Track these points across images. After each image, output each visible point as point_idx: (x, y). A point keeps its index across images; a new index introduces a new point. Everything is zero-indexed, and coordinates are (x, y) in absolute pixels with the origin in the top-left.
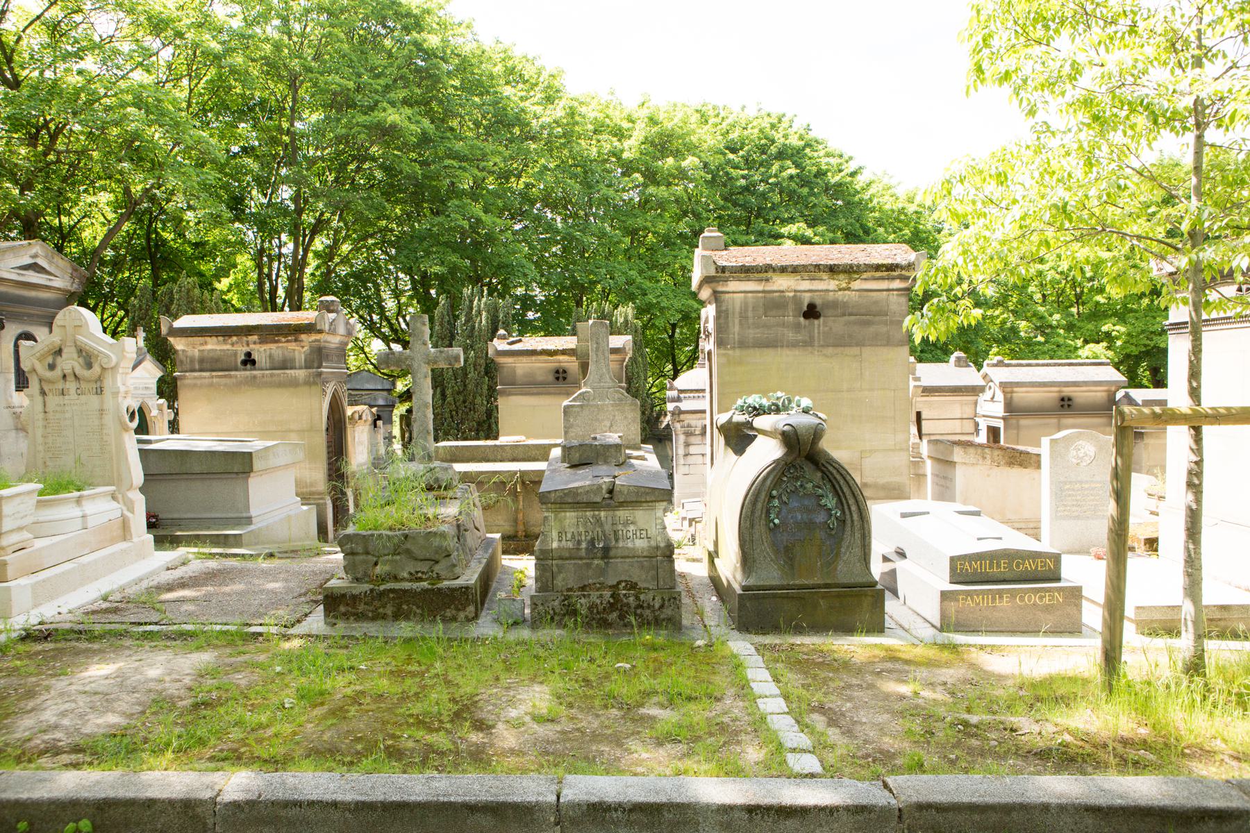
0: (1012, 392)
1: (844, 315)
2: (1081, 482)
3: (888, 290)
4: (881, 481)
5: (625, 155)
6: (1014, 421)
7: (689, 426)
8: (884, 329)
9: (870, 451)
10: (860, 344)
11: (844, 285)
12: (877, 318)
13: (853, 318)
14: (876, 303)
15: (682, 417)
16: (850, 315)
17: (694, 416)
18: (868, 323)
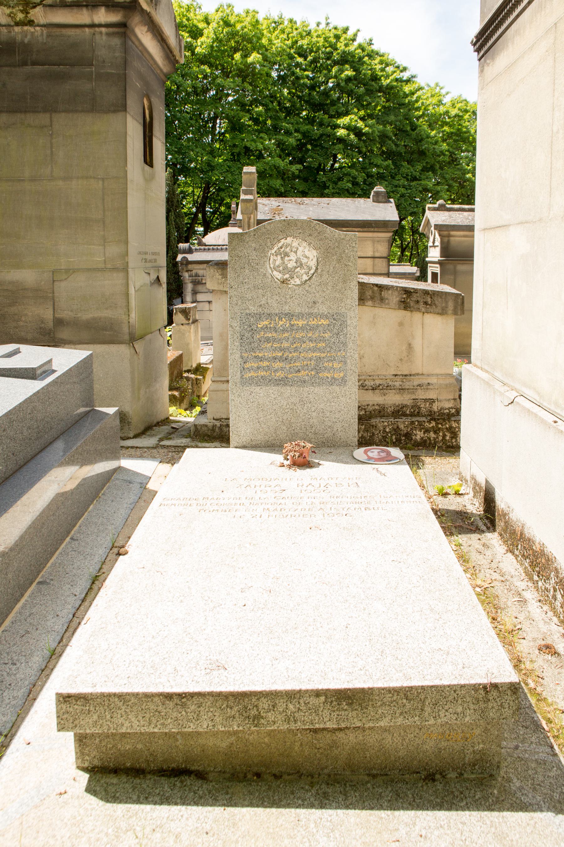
0: (449, 236)
1: (24, 63)
2: (290, 316)
3: (93, 26)
4: (86, 316)
5: (198, 50)
6: (450, 267)
7: (197, 275)
8: (87, 86)
9: (67, 271)
10: (51, 108)
11: (20, 16)
12: (76, 70)
13: (38, 68)
14: (75, 45)
15: (190, 267)
16: (34, 64)
17: (202, 266)
18: (62, 77)
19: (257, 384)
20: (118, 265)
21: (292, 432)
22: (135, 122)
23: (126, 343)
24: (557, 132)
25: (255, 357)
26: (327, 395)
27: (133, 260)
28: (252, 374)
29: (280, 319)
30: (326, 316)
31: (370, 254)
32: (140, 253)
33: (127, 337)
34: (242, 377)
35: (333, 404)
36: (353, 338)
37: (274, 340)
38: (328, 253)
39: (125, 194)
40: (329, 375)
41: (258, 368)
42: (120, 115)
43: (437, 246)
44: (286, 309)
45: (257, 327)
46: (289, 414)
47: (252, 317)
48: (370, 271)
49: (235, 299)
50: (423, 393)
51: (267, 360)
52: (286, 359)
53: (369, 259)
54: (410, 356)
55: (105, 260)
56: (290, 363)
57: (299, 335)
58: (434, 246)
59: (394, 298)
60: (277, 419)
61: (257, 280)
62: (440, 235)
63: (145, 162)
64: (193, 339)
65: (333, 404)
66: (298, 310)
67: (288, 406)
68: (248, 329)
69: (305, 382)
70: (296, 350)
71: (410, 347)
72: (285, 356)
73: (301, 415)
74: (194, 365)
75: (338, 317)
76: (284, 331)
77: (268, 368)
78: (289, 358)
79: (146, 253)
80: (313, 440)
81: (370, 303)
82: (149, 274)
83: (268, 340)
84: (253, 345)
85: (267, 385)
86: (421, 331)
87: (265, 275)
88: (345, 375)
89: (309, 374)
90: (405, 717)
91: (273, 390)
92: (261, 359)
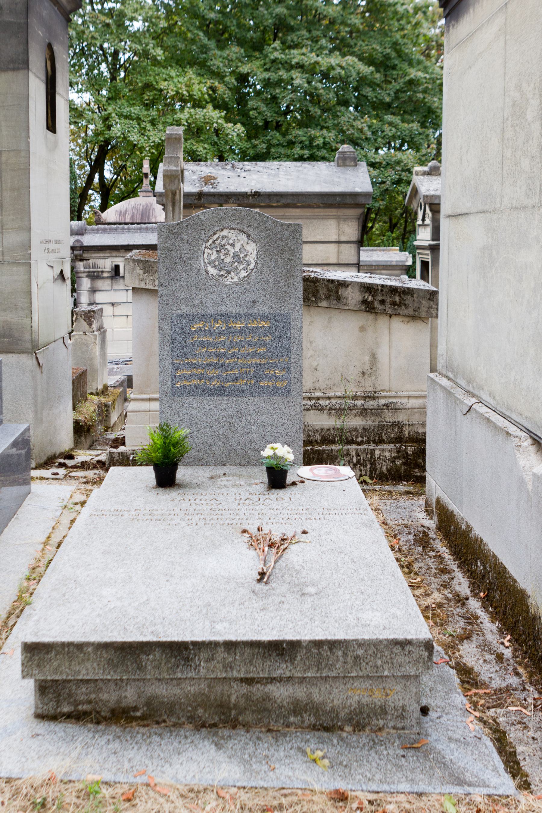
2: (226, 317)
19: (190, 394)
20: (19, 257)
21: (229, 448)
22: (37, 80)
23: (29, 353)
24: (507, 119)
25: (188, 363)
26: (268, 406)
27: (37, 253)
28: (185, 383)
29: (216, 320)
30: (267, 317)
31: (334, 238)
32: (43, 242)
33: (28, 345)
34: (173, 386)
35: (275, 416)
36: (297, 342)
37: (209, 344)
38: (269, 245)
39: (26, 171)
40: (270, 384)
41: (191, 376)
42: (21, 74)
43: (428, 225)
44: (223, 309)
45: (190, 330)
46: (225, 427)
47: (185, 318)
48: (334, 261)
49: (165, 298)
50: (391, 415)
51: (202, 367)
52: (222, 366)
53: (333, 244)
54: (374, 369)
55: (3, 251)
56: (227, 371)
57: (236, 339)
58: (423, 225)
59: (353, 297)
60: (213, 433)
61: (190, 276)
62: (431, 210)
63: (48, 128)
64: (98, 353)
65: (275, 416)
66: (236, 310)
67: (224, 419)
68: (180, 332)
69: (243, 392)
70: (233, 355)
71: (374, 357)
72: (221, 362)
73: (239, 429)
74: (100, 387)
75: (281, 318)
76: (220, 334)
77: (202, 377)
78: (226, 365)
79: (49, 242)
80: (252, 457)
81: (324, 304)
82: (52, 267)
83: (202, 345)
84: (185, 349)
85: (201, 395)
86: (387, 338)
87: (199, 271)
88: (289, 384)
89: (249, 383)
90: (330, 669)
91: (208, 402)
92: (195, 366)
